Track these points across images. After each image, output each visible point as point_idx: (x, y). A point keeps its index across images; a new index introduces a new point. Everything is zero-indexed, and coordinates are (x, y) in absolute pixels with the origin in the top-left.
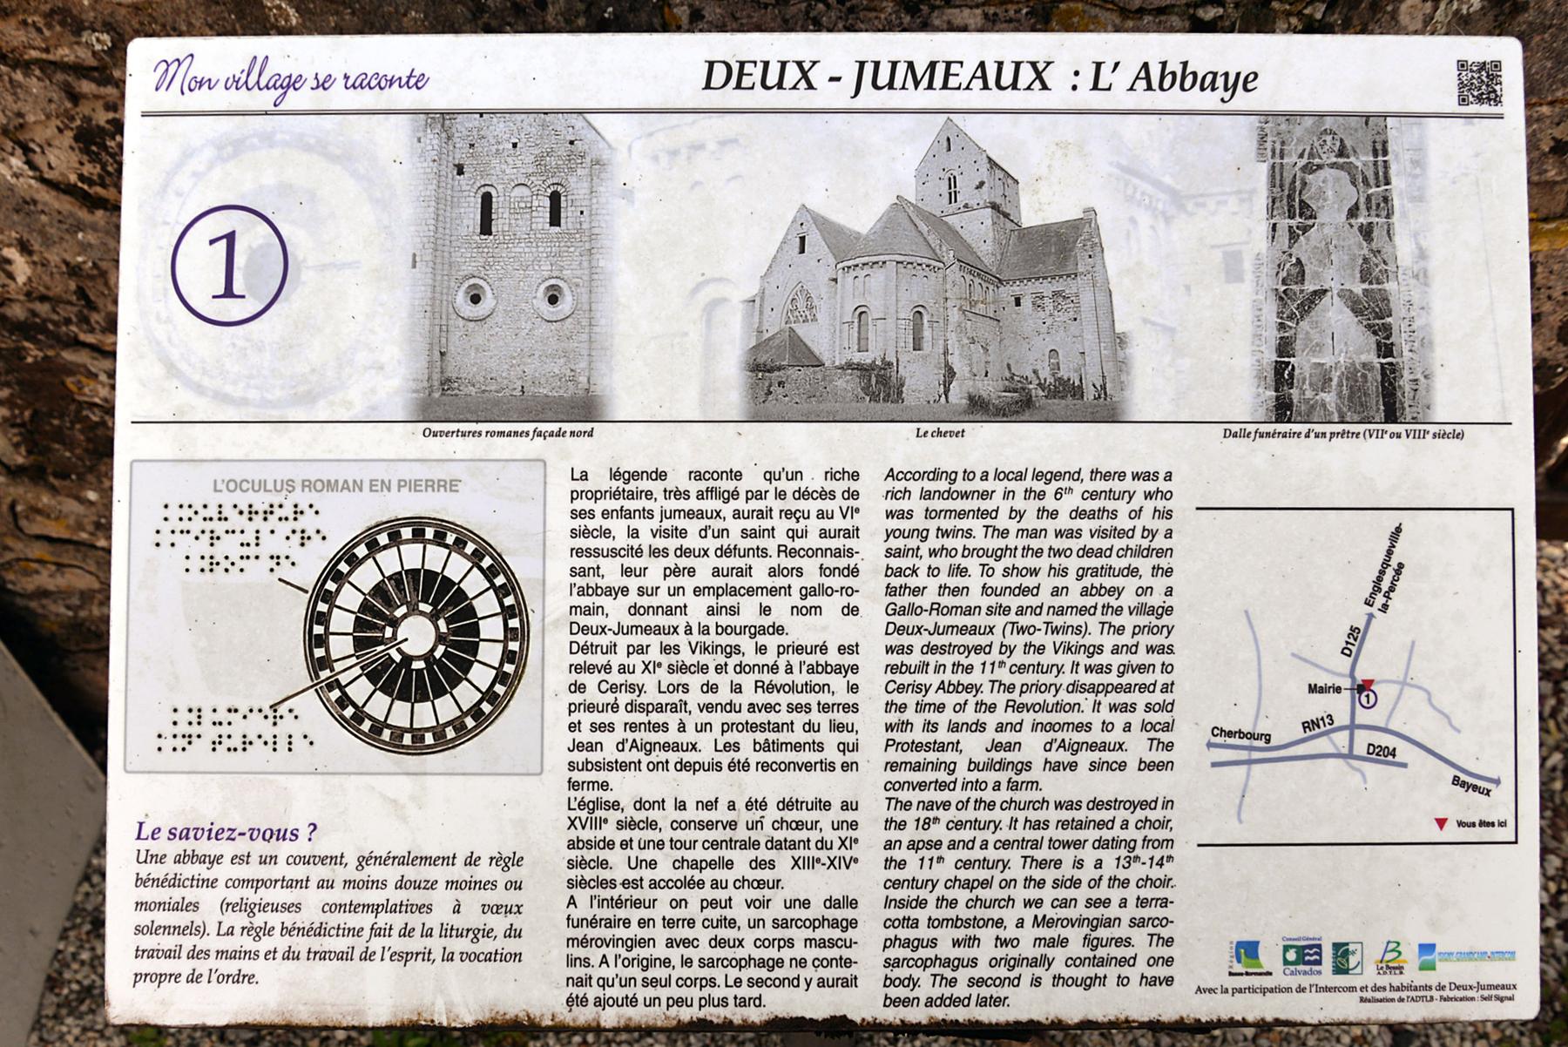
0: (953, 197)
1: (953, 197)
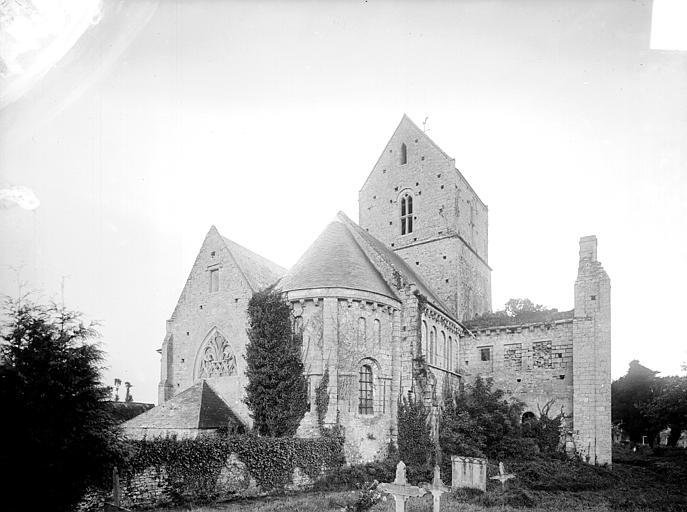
0: (407, 226)
1: (407, 226)
